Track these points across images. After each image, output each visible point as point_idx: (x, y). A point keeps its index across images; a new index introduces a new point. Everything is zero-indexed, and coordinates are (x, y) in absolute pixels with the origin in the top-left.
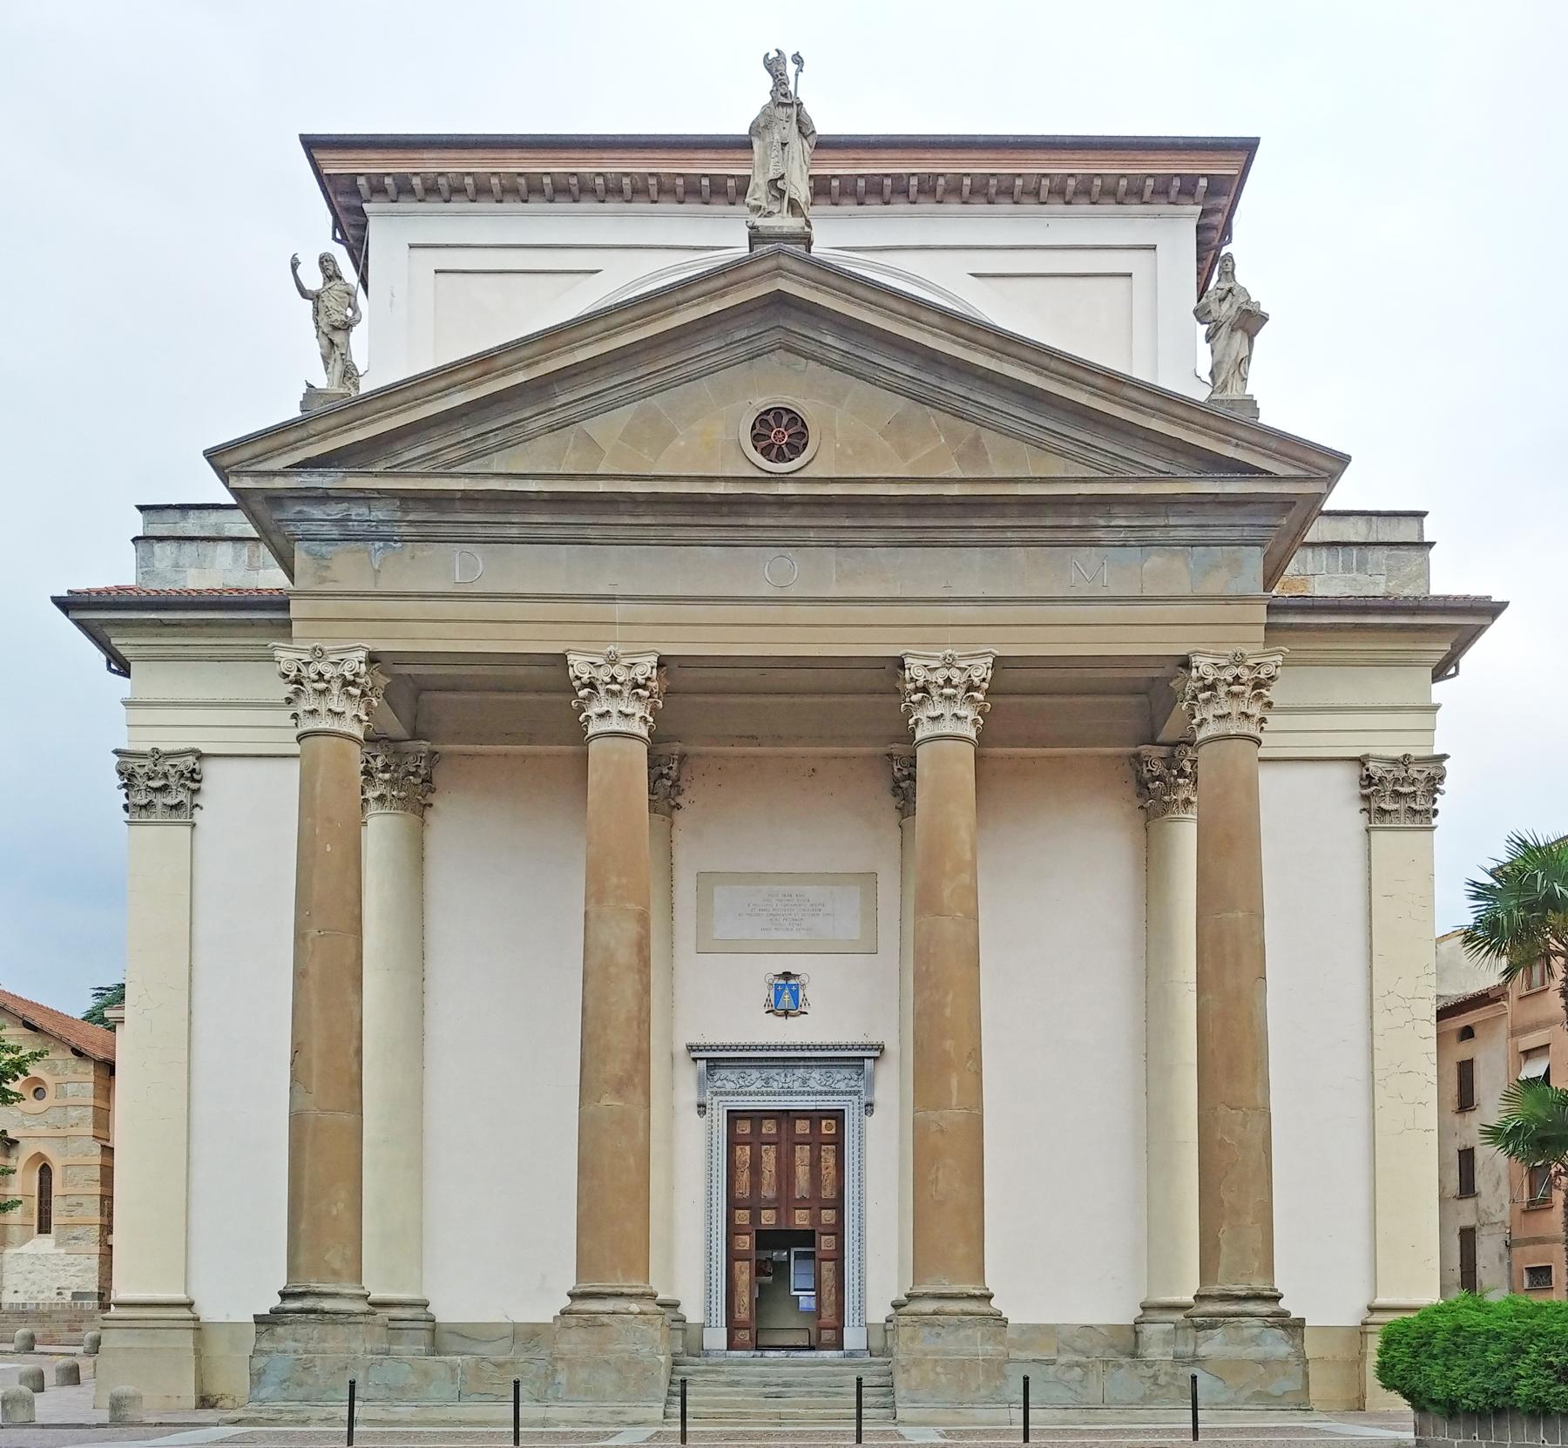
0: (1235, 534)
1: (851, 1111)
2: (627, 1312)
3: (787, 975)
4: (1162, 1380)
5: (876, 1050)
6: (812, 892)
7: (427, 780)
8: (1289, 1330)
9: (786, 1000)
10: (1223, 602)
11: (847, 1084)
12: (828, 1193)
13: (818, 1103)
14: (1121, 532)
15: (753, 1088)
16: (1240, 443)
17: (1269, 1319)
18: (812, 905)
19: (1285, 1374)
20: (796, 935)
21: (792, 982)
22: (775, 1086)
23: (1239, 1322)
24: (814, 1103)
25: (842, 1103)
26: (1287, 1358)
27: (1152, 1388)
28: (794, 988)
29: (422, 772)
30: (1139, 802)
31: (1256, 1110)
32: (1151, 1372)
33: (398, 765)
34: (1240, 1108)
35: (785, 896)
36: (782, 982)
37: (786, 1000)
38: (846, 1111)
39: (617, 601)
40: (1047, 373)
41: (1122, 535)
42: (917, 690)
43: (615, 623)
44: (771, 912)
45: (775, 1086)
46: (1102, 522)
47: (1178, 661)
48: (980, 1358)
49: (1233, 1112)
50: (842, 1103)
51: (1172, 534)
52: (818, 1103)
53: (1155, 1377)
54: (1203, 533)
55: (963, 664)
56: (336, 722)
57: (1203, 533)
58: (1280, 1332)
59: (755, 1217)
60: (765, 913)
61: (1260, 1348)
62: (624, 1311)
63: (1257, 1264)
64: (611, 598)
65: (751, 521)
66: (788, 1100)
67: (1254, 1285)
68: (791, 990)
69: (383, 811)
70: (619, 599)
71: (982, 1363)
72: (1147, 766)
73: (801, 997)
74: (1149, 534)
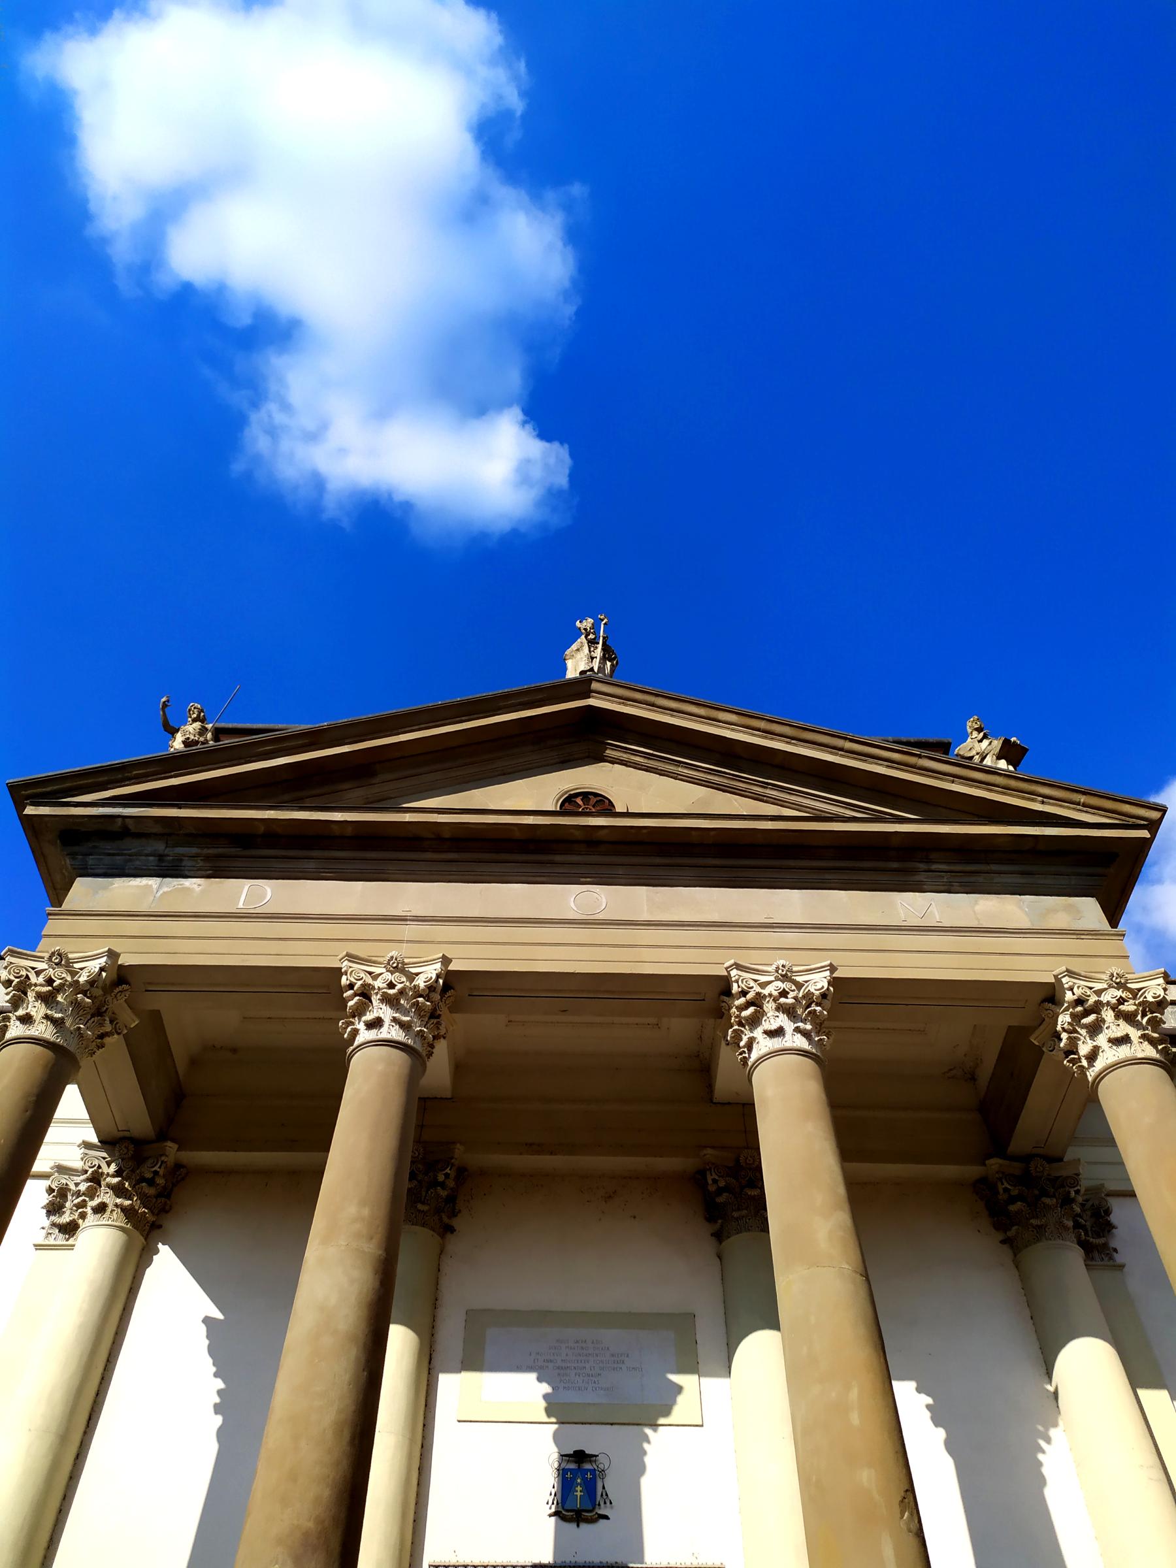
6: (610, 1336)
7: (452, 1199)
9: (579, 1494)
10: (1075, 937)
16: (1045, 800)
18: (613, 1355)
20: (590, 1397)
21: (587, 1466)
28: (589, 1476)
30: (1001, 1236)
33: (133, 1171)
35: (577, 1342)
36: (572, 1466)
37: (579, 1494)
39: (408, 923)
40: (842, 753)
42: (749, 1004)
43: (408, 941)
46: (922, 866)
47: (1041, 995)
55: (800, 979)
60: (551, 1365)
65: (558, 858)
68: (584, 1479)
69: (100, 1223)
70: (410, 920)
73: (599, 1490)
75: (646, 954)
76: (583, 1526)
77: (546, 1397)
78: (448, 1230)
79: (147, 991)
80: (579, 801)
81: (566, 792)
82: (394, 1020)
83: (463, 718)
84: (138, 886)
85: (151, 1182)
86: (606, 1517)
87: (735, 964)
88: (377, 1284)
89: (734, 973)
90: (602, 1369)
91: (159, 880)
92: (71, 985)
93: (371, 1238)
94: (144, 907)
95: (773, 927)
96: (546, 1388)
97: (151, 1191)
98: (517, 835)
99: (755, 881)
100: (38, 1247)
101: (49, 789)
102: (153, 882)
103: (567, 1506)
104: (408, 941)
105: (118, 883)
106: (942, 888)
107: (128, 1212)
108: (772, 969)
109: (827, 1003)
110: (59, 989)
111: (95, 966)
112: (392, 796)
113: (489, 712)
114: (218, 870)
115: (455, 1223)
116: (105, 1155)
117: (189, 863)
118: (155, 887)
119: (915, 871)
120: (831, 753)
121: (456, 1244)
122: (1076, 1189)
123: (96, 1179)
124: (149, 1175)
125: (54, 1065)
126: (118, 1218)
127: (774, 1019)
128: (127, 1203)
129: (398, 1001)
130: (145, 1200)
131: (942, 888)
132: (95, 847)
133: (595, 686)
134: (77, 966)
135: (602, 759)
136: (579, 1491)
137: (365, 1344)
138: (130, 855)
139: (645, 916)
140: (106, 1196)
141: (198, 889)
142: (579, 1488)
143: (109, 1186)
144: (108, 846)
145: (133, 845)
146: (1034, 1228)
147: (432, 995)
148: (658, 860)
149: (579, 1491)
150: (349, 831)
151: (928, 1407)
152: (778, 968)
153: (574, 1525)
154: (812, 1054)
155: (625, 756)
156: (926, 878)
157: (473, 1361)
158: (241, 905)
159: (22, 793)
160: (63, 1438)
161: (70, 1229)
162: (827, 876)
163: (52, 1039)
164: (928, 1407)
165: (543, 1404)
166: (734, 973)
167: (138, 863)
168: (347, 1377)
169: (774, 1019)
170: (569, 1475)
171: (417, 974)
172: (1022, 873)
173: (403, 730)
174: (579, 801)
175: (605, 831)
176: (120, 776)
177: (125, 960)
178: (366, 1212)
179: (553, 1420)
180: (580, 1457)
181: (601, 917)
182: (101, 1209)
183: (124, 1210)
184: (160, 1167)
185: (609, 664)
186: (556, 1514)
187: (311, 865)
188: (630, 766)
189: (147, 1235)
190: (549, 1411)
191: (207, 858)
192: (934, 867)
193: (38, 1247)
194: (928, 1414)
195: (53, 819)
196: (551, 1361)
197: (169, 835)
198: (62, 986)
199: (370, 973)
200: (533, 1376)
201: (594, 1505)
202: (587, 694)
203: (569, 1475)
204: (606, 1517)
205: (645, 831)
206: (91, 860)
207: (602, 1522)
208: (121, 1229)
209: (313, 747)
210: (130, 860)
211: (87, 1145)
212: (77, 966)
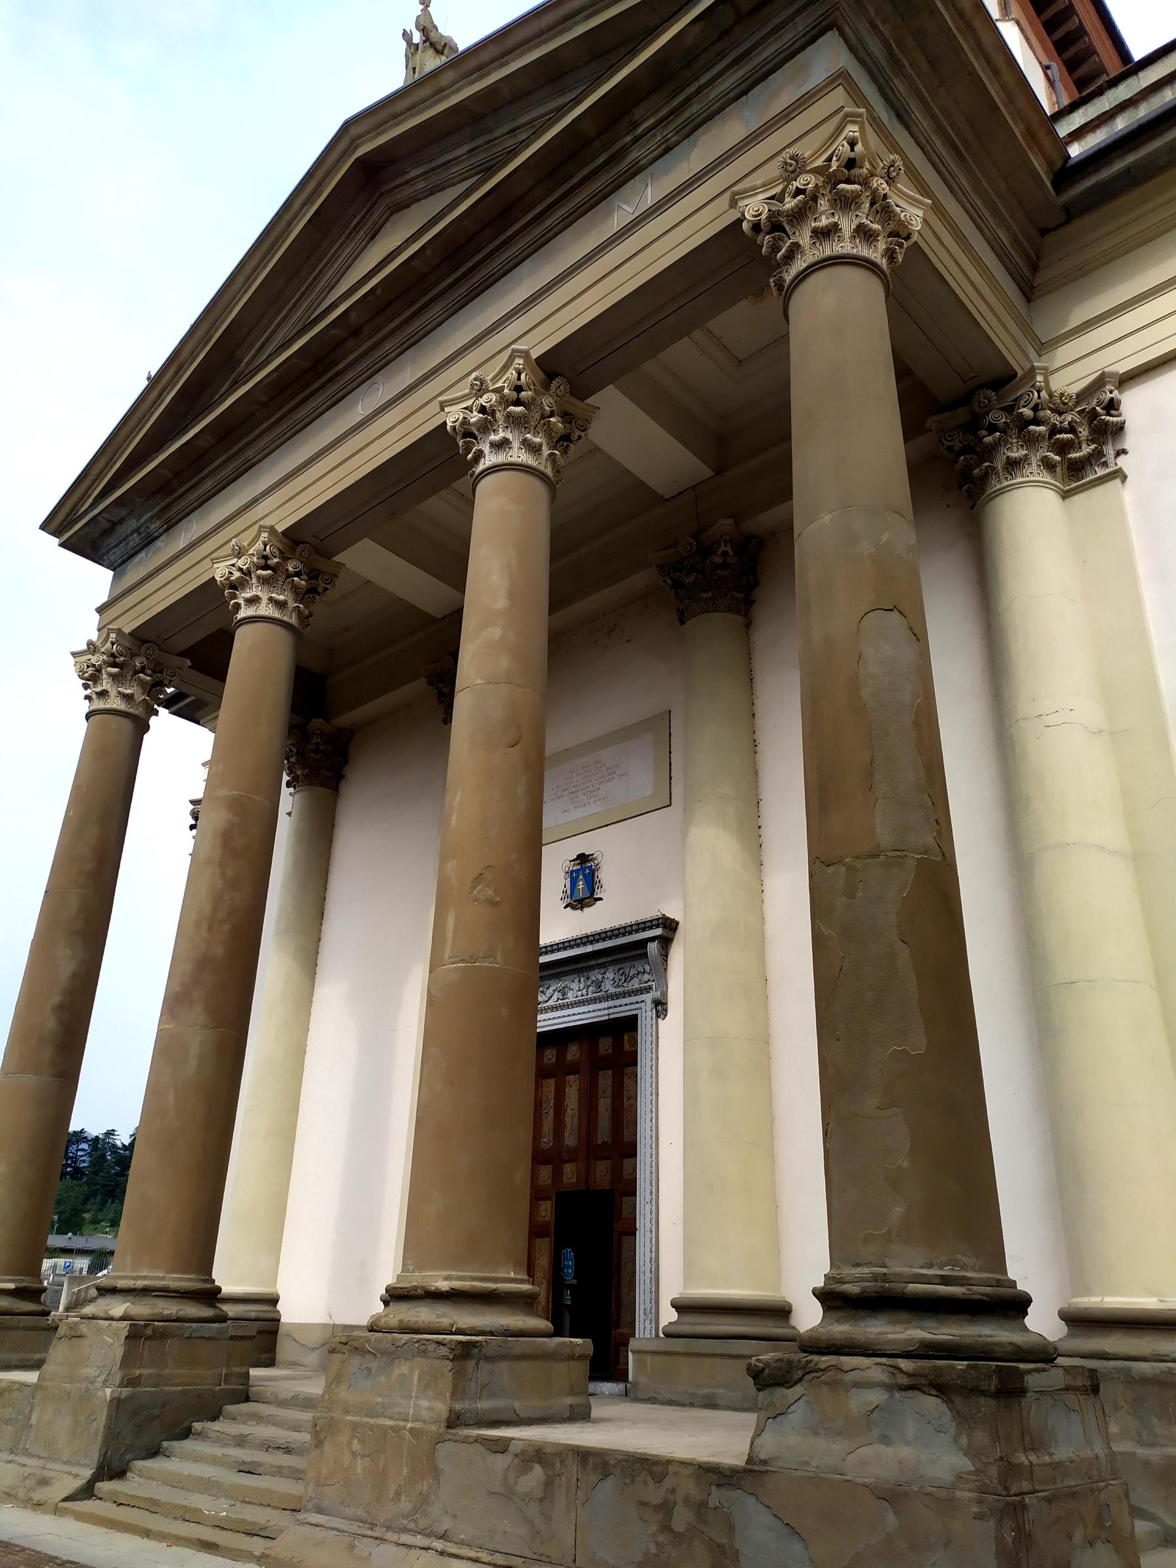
0: (788, 37)
1: (644, 1014)
2: (105, 1316)
3: (583, 858)
4: (682, 1518)
5: (657, 926)
8: (957, 1400)
9: (581, 887)
11: (640, 980)
12: (603, 1133)
13: (611, 1011)
14: (655, 136)
15: (551, 1003)
17: (903, 1364)
19: (948, 1544)
22: (571, 997)
23: (838, 1368)
24: (606, 1012)
25: (633, 1007)
26: (954, 1487)
27: (660, 1539)
28: (587, 871)
31: (878, 856)
32: (655, 1494)
34: (840, 862)
38: (639, 1016)
41: (659, 138)
44: (572, 789)
45: (571, 997)
48: (409, 1425)
49: (831, 870)
50: (633, 1007)
51: (713, 95)
52: (611, 1011)
53: (666, 1508)
54: (748, 67)
56: (101, 702)
57: (748, 67)
58: (931, 1403)
59: (557, 1174)
61: (889, 1451)
62: (102, 1315)
63: (898, 1211)
66: (571, 1013)
67: (897, 1267)
70: (261, 498)
71: (408, 1435)
72: (943, 444)
74: (687, 114)
76: (586, 910)
78: (749, 602)
79: (165, 640)
82: (271, 599)
86: (601, 899)
90: (600, 783)
99: (693, 120)
119: (624, 151)
120: (413, 116)
122: (720, 552)
132: (108, 545)
136: (581, 885)
142: (581, 883)
146: (704, 601)
149: (581, 885)
153: (579, 911)
154: (548, 477)
156: (639, 151)
172: (737, 62)
184: (726, 546)
195: (488, 199)
196: (566, 790)
201: (592, 891)
204: (601, 899)
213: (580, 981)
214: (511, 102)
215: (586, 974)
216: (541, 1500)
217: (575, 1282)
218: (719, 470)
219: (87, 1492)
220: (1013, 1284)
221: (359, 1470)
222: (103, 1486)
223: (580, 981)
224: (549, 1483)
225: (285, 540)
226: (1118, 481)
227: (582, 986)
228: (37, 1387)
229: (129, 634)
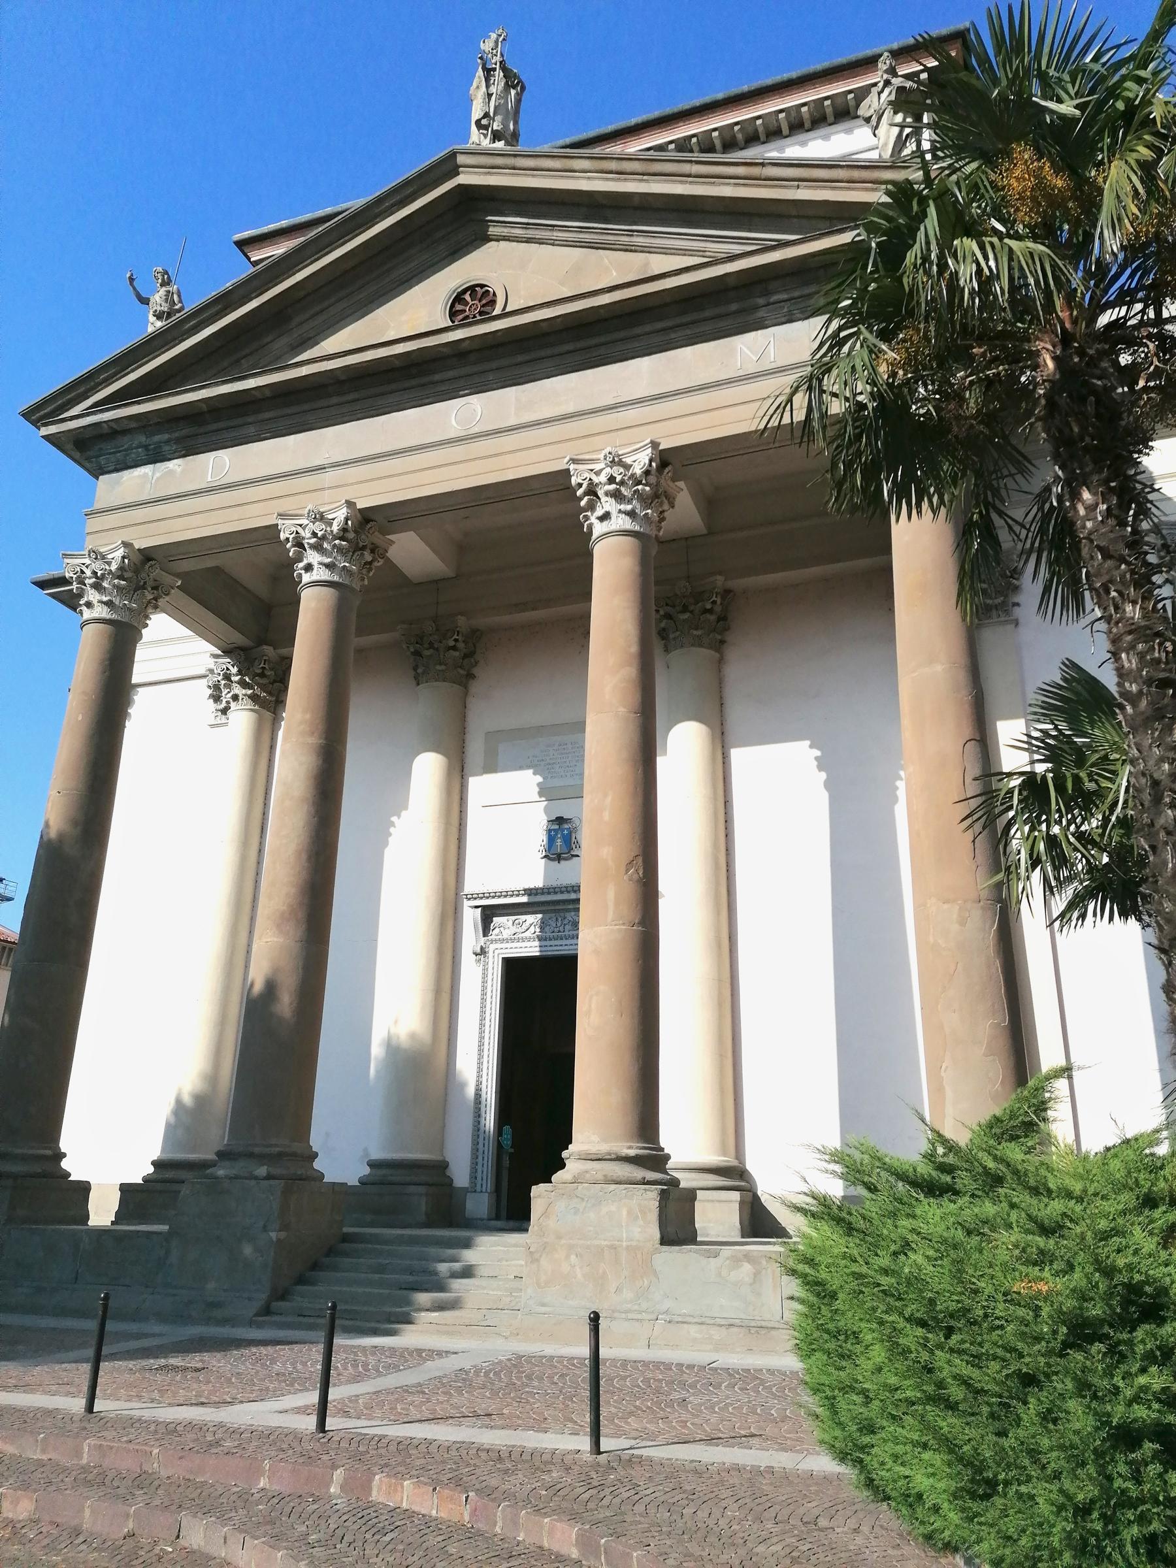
21: (566, 826)
28: (566, 832)
29: (718, 608)
43: (330, 488)
46: (761, 301)
60: (542, 763)
64: (321, 468)
65: (437, 377)
68: (563, 835)
75: (509, 460)
76: (562, 862)
77: (539, 784)
78: (470, 676)
80: (459, 307)
81: (454, 291)
83: (346, 238)
84: (139, 476)
85: (262, 675)
86: (578, 856)
87: (571, 459)
88: (320, 762)
89: (572, 467)
91: (151, 466)
92: (109, 574)
93: (313, 733)
94: (144, 497)
95: (616, 407)
96: (539, 779)
97: (264, 681)
98: (397, 363)
100: (212, 726)
101: (48, 409)
102: (147, 470)
103: (552, 852)
104: (330, 488)
105: (127, 475)
106: (783, 319)
107: (254, 698)
108: (601, 456)
109: (652, 479)
110: (103, 577)
111: (120, 553)
112: (311, 335)
113: (367, 223)
114: (189, 449)
115: (475, 671)
116: (229, 660)
117: (166, 448)
118: (150, 474)
119: (757, 308)
121: (475, 687)
123: (227, 677)
124: (259, 671)
125: (116, 635)
126: (249, 704)
127: (607, 504)
128: (629, 507)
129: (321, 546)
130: (263, 687)
131: (783, 319)
132: (101, 449)
133: (461, 159)
134: (110, 556)
135: (487, 239)
136: (559, 842)
137: (313, 802)
138: (125, 450)
139: (513, 421)
140: (237, 690)
141: (179, 470)
143: (607, 494)
144: (108, 447)
145: (125, 441)
147: (347, 535)
148: (520, 358)
149: (559, 842)
150: (268, 393)
151: (816, 758)
152: (605, 456)
155: (506, 230)
157: (491, 766)
158: (209, 479)
159: (38, 414)
160: (245, 843)
161: (224, 711)
162: (673, 336)
163: (108, 617)
164: (816, 758)
165: (537, 789)
166: (572, 467)
167: (133, 456)
168: (301, 824)
169: (607, 504)
170: (553, 833)
171: (333, 519)
173: (297, 268)
174: (459, 307)
175: (467, 342)
176: (92, 384)
177: (138, 545)
178: (308, 716)
179: (543, 799)
180: (560, 820)
181: (476, 430)
182: (235, 698)
183: (250, 697)
185: (513, 92)
186: (545, 857)
187: (251, 430)
188: (513, 241)
189: (275, 709)
190: (541, 794)
191: (178, 441)
192: (775, 298)
193: (212, 726)
194: (816, 763)
197: (144, 427)
198: (103, 575)
199: (301, 525)
200: (531, 771)
202: (454, 172)
203: (553, 833)
204: (578, 856)
205: (500, 333)
206: (102, 460)
207: (575, 859)
208: (251, 710)
209: (227, 311)
210: (127, 455)
211: (216, 656)
212: (110, 556)
213: (557, 920)
214: (636, 208)
215: (562, 914)
216: (751, 1285)
217: (512, 1150)
218: (711, 533)
219: (267, 1311)
220: (663, 1150)
221: (579, 1276)
222: (276, 1305)
223: (557, 920)
224: (757, 1274)
225: (359, 515)
226: (1013, 626)
227: (559, 925)
228: (167, 1237)
229: (139, 550)
